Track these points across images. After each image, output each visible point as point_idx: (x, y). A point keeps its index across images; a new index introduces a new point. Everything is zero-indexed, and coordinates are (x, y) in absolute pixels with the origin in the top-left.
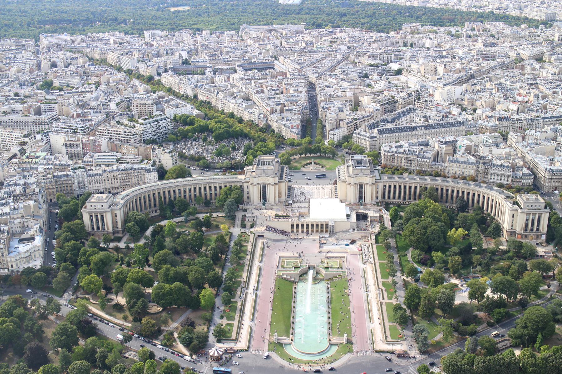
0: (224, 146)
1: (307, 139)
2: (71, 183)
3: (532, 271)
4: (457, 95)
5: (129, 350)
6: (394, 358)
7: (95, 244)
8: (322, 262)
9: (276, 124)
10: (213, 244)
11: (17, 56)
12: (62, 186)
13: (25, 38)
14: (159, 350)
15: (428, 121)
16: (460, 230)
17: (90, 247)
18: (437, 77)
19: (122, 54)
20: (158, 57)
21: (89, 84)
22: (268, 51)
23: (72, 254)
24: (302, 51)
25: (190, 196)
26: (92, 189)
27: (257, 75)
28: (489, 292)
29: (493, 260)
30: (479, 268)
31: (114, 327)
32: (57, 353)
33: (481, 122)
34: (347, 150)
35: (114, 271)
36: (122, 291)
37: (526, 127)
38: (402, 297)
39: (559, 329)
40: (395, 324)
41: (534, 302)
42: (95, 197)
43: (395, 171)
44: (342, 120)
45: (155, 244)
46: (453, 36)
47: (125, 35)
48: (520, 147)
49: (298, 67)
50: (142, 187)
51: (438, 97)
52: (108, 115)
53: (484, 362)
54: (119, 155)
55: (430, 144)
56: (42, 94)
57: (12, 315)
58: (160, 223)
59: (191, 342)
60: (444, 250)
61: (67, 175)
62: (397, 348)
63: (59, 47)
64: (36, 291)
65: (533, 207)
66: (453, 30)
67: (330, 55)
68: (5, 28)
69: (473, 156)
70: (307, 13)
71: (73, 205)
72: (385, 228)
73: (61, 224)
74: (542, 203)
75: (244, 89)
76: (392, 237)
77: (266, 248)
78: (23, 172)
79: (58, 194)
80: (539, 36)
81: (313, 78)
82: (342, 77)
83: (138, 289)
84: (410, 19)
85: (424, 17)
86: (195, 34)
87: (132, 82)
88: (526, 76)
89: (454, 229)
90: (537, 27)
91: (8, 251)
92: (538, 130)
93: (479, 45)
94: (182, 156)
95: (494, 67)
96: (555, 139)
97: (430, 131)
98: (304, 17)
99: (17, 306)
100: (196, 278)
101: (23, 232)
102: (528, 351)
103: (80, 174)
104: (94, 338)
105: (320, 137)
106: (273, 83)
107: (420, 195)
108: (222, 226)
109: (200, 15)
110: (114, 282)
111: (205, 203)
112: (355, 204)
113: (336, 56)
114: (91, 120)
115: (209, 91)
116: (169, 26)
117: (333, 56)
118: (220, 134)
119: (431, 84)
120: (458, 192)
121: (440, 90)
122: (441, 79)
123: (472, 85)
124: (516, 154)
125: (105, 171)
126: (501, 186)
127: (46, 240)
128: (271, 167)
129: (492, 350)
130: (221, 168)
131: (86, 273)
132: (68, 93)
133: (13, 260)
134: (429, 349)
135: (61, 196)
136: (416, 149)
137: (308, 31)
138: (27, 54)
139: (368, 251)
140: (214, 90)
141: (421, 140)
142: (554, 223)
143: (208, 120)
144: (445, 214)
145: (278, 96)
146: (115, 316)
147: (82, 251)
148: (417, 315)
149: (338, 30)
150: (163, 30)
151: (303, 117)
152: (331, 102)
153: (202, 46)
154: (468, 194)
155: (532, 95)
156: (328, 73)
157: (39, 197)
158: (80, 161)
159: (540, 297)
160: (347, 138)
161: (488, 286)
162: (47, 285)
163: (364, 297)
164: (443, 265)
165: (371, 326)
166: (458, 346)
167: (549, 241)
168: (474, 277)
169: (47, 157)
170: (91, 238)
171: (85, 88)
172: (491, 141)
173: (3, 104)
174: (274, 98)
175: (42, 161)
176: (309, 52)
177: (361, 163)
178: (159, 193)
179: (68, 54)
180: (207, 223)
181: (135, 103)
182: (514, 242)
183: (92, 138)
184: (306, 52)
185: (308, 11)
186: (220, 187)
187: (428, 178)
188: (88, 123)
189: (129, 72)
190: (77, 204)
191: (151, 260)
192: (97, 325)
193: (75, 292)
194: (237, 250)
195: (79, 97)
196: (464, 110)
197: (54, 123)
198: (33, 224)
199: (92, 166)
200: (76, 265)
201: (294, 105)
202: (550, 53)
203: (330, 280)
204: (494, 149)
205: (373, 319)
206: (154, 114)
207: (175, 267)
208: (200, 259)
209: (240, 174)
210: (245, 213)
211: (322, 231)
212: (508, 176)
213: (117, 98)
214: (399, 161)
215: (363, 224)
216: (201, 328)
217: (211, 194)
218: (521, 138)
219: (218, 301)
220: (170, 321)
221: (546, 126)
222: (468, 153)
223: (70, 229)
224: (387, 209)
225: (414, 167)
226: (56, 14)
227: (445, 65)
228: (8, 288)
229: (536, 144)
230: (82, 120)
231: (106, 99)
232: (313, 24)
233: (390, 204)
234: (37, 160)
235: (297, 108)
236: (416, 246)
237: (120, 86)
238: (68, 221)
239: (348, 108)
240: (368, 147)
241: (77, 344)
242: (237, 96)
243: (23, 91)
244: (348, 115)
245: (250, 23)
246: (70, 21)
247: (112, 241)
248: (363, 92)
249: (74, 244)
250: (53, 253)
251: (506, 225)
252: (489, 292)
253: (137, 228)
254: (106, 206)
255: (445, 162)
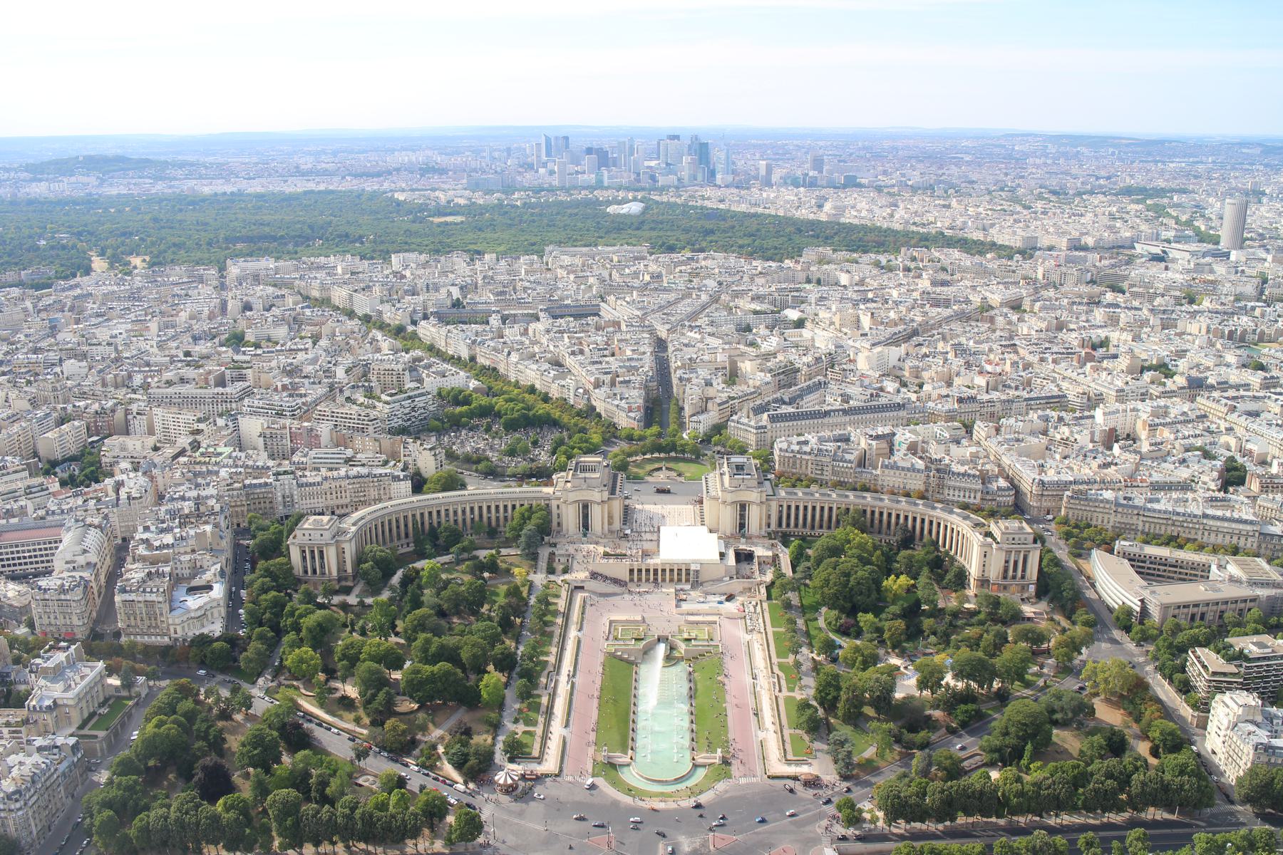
0: (519, 440)
1: (655, 429)
2: (272, 498)
3: (1016, 643)
4: (893, 361)
5: (363, 772)
6: (798, 786)
7: (310, 598)
8: (681, 631)
9: (603, 404)
10: (501, 600)
11: (190, 292)
12: (257, 501)
13: (203, 264)
14: (411, 771)
15: (848, 402)
16: (903, 578)
17: (301, 602)
18: (860, 332)
19: (356, 291)
20: (413, 295)
21: (302, 338)
22: (590, 287)
23: (271, 613)
24: (644, 288)
25: (464, 520)
26: (305, 507)
27: (572, 325)
28: (949, 679)
29: (955, 626)
30: (933, 639)
31: (339, 734)
32: (247, 776)
33: (931, 404)
34: (719, 448)
35: (340, 643)
36: (353, 675)
37: (1000, 414)
38: (810, 687)
39: (1057, 735)
40: (798, 731)
41: (1018, 694)
42: (310, 521)
43: (797, 481)
44: (711, 399)
45: (407, 598)
46: (882, 268)
47: (361, 259)
48: (992, 445)
49: (639, 313)
50: (386, 504)
51: (862, 364)
52: (332, 387)
53: (942, 791)
54: (349, 452)
55: (852, 439)
56: (228, 353)
57: (174, 712)
58: (415, 565)
59: (466, 761)
60: (877, 611)
61: (266, 484)
62: (803, 770)
63: (257, 279)
64: (213, 673)
65: (1016, 541)
66: (883, 259)
67: (689, 295)
68: (173, 249)
69: (921, 458)
70: (652, 229)
71: (274, 533)
72: (783, 575)
73: (254, 564)
74: (1029, 534)
75: (552, 348)
76: (793, 590)
77: (588, 607)
78: (194, 478)
79: (251, 514)
80: (1014, 272)
81: (662, 331)
82: (709, 329)
83: (378, 672)
84: (816, 241)
85: (836, 238)
86: (472, 260)
87: (371, 335)
88: (998, 333)
89: (893, 576)
90: (1010, 258)
91: (170, 606)
92: (1020, 418)
93: (924, 283)
94: (451, 456)
95: (949, 317)
96: (1045, 433)
97: (852, 417)
98: (647, 234)
99: (182, 698)
100: (473, 655)
101: (193, 576)
102: (1011, 771)
103: (286, 482)
104: (306, 752)
105: (676, 427)
106: (599, 339)
107: (838, 522)
108: (516, 571)
109: (480, 230)
110: (340, 660)
111: (488, 533)
112: (732, 536)
113: (699, 297)
114: (305, 395)
115: (495, 349)
116: (431, 247)
117: (694, 296)
118: (512, 420)
119: (850, 342)
120: (898, 516)
121: (866, 353)
122: (866, 335)
123: (916, 346)
124: (987, 457)
125: (326, 479)
126: (965, 507)
127: (230, 590)
128: (597, 475)
129: (955, 771)
130: (514, 476)
131: (293, 645)
132: (268, 352)
133: (178, 621)
134: (855, 772)
135: (255, 517)
136: (831, 446)
137: (653, 257)
138: (206, 290)
139: (755, 612)
140: (503, 348)
141: (837, 432)
142: (1048, 565)
143: (494, 396)
144: (878, 552)
145: (607, 359)
146: (341, 718)
147: (288, 608)
148: (836, 717)
149: (702, 255)
150: (421, 253)
151: (647, 394)
152: (693, 370)
153: (484, 278)
154: (915, 519)
155: (1008, 362)
156: (687, 323)
157: (221, 519)
158: (287, 462)
159: (1028, 685)
160: (719, 428)
161: (946, 667)
162: (231, 663)
163: (749, 689)
164: (875, 635)
165: (761, 735)
166: (901, 767)
167: (1040, 594)
168: (925, 654)
169: (234, 454)
170: (303, 587)
171: (296, 344)
172: (947, 435)
173: (167, 368)
174: (601, 363)
175: (226, 461)
176: (656, 289)
177: (743, 469)
178: (414, 516)
179: (270, 290)
180: (492, 566)
181: (376, 368)
182: (987, 597)
183: (306, 424)
184: (651, 290)
185: (653, 226)
186: (514, 507)
187: (851, 494)
188: (300, 401)
189: (367, 319)
190: (281, 532)
191: (400, 625)
192: (312, 731)
193: (275, 676)
194: (541, 610)
195: (287, 358)
196: (904, 385)
197: (246, 400)
198: (211, 563)
199: (305, 469)
200: (279, 632)
201: (633, 374)
202: (1032, 298)
203: (693, 658)
204: (953, 447)
205: (764, 723)
206: (406, 387)
207: (440, 637)
208: (480, 624)
209: (546, 485)
210: (554, 549)
211: (680, 580)
212: (976, 491)
213: (347, 360)
214: (804, 467)
215: (745, 567)
216: (481, 739)
217: (498, 518)
218: (993, 430)
219: (510, 694)
220: (431, 726)
221: (1031, 412)
222: (913, 454)
223: (268, 573)
224: (786, 544)
225: (828, 476)
226: (253, 227)
227: (872, 314)
228: (169, 666)
229: (1018, 440)
230: (291, 396)
231: (330, 363)
232: (661, 246)
233: (790, 536)
234: (218, 460)
235: (637, 379)
236: (833, 604)
237: (352, 342)
238: (267, 560)
239: (720, 380)
240: (753, 443)
241: (279, 762)
242: (540, 358)
243: (197, 348)
244: (720, 390)
245: (561, 242)
246: (274, 239)
247: (337, 592)
248: (743, 354)
249: (275, 597)
250: (241, 611)
251: (974, 570)
252: (949, 679)
253: (377, 573)
254: (327, 535)
255: (876, 468)
